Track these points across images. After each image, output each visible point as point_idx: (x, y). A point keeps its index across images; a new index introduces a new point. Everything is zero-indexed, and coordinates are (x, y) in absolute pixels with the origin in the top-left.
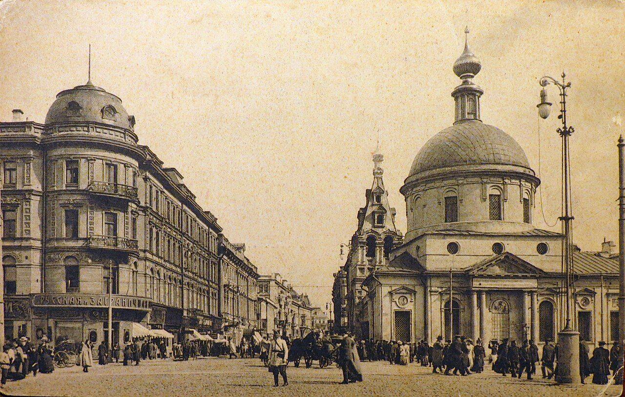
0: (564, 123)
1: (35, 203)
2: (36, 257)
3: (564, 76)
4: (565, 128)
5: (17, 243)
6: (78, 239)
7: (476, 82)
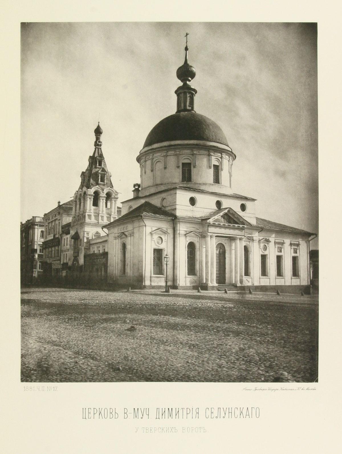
7: (192, 84)
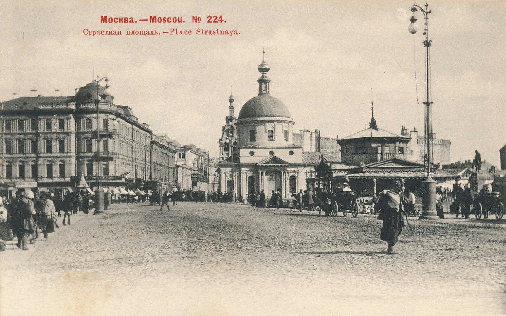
0: (427, 38)
1: (73, 136)
2: (74, 160)
3: (427, 6)
4: (427, 41)
5: (65, 155)
6: (91, 152)
7: (268, 75)
